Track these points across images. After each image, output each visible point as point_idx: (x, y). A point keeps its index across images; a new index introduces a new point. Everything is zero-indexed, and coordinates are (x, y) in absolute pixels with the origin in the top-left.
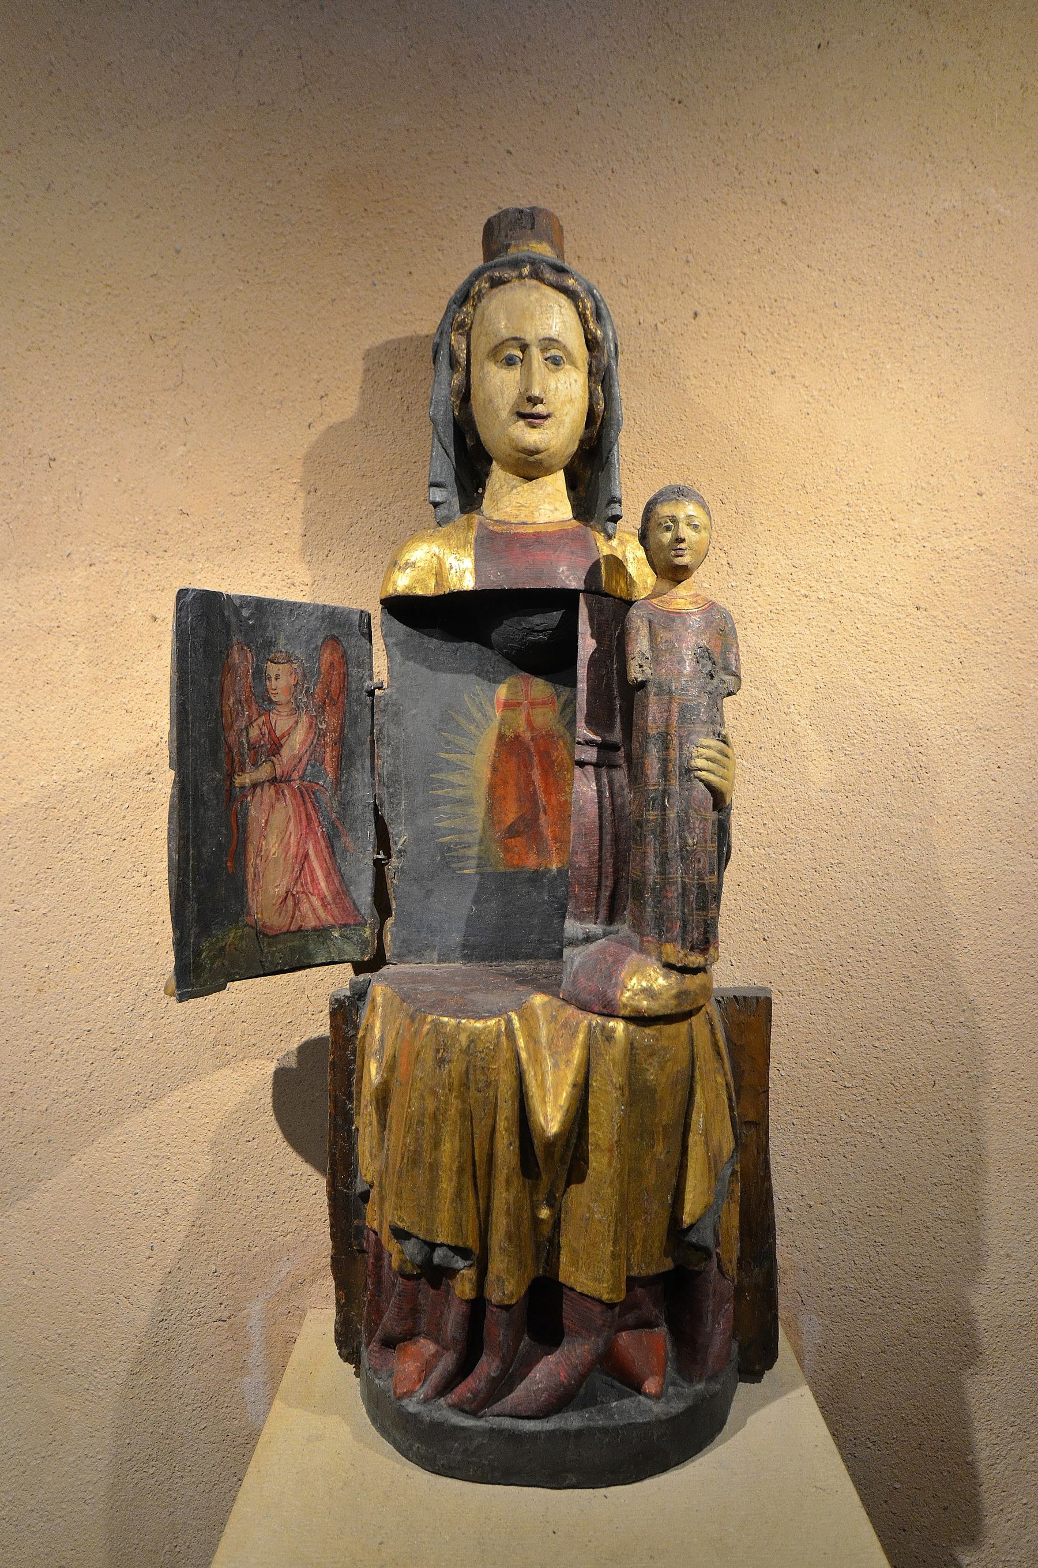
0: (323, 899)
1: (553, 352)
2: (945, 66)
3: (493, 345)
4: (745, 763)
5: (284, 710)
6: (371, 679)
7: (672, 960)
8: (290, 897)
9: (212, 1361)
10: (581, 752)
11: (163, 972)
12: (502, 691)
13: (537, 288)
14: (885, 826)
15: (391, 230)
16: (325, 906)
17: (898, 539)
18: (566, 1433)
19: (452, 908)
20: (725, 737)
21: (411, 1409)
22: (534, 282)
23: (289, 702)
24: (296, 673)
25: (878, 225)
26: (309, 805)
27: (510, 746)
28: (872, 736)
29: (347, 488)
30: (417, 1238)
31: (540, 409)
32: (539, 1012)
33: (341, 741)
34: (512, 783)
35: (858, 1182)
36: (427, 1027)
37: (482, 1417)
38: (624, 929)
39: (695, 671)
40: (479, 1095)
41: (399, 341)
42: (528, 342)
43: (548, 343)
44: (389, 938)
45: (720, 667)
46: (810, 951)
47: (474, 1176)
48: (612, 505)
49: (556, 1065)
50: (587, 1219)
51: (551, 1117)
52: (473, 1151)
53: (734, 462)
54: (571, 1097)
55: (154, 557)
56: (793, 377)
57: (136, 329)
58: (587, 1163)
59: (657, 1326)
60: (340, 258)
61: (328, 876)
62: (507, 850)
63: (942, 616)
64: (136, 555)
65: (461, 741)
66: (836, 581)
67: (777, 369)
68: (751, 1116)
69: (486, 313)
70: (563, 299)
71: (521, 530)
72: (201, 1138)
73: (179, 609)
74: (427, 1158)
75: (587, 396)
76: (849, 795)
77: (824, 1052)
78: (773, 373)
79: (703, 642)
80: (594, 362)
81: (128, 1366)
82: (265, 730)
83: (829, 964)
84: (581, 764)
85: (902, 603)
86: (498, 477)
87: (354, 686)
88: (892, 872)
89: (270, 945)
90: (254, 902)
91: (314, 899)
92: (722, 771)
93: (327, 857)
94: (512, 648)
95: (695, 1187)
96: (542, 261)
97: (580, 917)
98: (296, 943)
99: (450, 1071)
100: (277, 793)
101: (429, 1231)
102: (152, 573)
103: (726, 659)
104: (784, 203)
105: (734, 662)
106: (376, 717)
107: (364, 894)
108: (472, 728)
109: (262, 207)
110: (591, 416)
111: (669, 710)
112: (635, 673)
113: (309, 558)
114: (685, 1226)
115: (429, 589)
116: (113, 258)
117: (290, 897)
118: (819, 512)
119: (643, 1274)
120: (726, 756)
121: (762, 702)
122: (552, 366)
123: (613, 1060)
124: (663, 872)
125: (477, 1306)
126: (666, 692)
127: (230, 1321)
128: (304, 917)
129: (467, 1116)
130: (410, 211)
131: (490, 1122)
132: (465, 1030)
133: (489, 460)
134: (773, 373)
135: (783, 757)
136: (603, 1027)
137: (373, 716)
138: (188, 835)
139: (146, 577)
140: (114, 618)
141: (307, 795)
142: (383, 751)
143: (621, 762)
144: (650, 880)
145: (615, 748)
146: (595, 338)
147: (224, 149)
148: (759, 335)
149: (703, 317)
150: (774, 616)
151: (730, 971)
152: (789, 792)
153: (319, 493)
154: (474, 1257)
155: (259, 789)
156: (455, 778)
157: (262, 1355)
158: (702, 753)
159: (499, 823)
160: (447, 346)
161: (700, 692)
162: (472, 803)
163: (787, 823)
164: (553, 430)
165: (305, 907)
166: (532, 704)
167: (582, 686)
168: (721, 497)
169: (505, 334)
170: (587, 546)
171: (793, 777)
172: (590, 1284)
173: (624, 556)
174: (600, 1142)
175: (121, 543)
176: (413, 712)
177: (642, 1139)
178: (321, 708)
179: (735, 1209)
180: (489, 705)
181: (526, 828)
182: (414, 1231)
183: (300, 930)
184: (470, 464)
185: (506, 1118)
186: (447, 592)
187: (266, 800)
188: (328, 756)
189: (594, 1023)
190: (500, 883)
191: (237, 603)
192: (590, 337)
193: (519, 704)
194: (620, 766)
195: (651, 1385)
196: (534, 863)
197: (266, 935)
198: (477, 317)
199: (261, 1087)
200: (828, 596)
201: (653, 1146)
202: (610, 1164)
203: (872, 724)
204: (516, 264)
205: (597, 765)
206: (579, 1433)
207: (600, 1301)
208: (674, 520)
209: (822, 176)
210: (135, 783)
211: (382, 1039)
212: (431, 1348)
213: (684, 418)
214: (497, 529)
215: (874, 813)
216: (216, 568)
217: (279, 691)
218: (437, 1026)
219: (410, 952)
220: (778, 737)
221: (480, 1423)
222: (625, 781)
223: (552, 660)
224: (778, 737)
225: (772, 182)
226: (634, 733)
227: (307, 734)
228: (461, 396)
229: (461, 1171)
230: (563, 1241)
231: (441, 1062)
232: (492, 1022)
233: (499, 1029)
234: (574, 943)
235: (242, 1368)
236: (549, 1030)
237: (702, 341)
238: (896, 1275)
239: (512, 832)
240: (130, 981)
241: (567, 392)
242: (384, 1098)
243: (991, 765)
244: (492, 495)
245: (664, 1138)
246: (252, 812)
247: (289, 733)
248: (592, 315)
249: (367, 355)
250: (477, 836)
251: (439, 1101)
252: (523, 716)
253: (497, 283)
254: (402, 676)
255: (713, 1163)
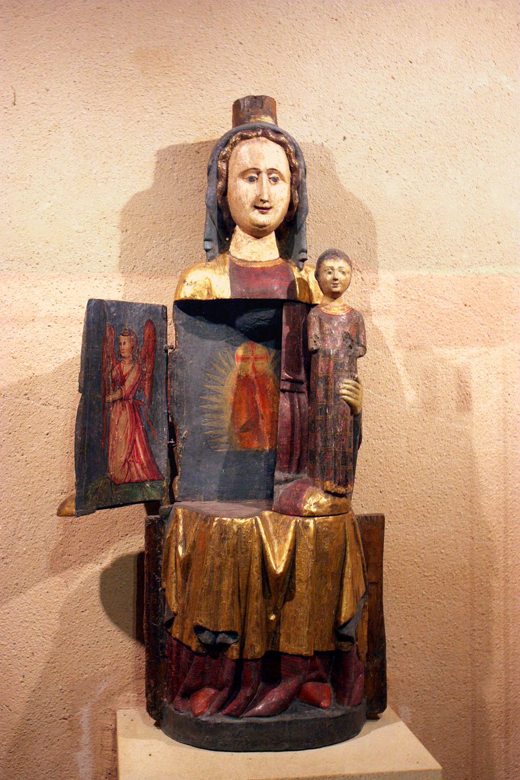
0: (142, 465)
1: (274, 175)
2: (479, 9)
3: (242, 170)
4: (370, 391)
5: (127, 361)
6: (167, 343)
7: (329, 489)
8: (127, 464)
9: (58, 743)
10: (284, 385)
11: (32, 512)
12: (240, 352)
13: (266, 142)
14: (447, 428)
15: (173, 83)
16: (142, 469)
17: (455, 266)
18: (284, 722)
19: (212, 472)
20: (357, 378)
21: (204, 719)
22: (264, 139)
23: (129, 357)
24: (133, 341)
25: (444, 93)
26: (137, 413)
27: (244, 381)
28: (440, 377)
29: (145, 230)
30: (209, 630)
31: (267, 205)
32: (268, 519)
33: (152, 379)
34: (244, 402)
35: (432, 630)
36: (215, 524)
37: (242, 718)
38: (305, 476)
39: (343, 345)
40: (242, 555)
41: (177, 146)
42: (261, 171)
43: (271, 171)
44: (177, 487)
45: (355, 339)
46: (406, 498)
47: (239, 597)
48: (302, 253)
49: (279, 542)
50: (295, 617)
51: (278, 566)
52: (239, 584)
53: (365, 221)
54: (288, 556)
55: (30, 267)
56: (398, 174)
57: (22, 134)
58: (295, 590)
59: (326, 682)
60: (142, 97)
61: (145, 453)
62: (241, 439)
63: (480, 311)
64: (19, 266)
65: (218, 378)
66: (421, 289)
67: (389, 170)
68: (374, 579)
69: (239, 153)
70: (278, 147)
71: (254, 266)
72: (54, 611)
73: (88, 310)
74: (215, 588)
75: (290, 195)
76: (428, 410)
77: (414, 556)
78: (387, 172)
79: (347, 330)
80: (294, 179)
81: (7, 747)
82: (119, 372)
83: (417, 506)
84: (284, 391)
85: (457, 302)
86: (239, 236)
87: (158, 347)
88: (451, 453)
89: (116, 489)
90: (111, 466)
91: (138, 465)
92: (355, 396)
93: (145, 442)
94: (247, 328)
95: (347, 604)
96: (268, 128)
97: (282, 470)
98: (127, 489)
99: (228, 544)
100: (123, 406)
101: (216, 626)
102: (29, 277)
103: (358, 338)
104: (393, 78)
105: (363, 340)
106: (169, 364)
107: (163, 463)
108: (223, 371)
109: (98, 67)
110: (291, 205)
111: (329, 365)
112: (312, 346)
113: (123, 270)
114: (342, 624)
115: (204, 296)
116: (9, 92)
117: (127, 464)
118: (412, 251)
119: (320, 650)
120: (358, 388)
121: (380, 357)
122: (272, 182)
123: (309, 538)
124: (325, 446)
125: (240, 663)
126: (326, 354)
127: (69, 719)
128: (132, 474)
129: (236, 565)
130: (184, 74)
131: (248, 569)
132: (235, 523)
133: (235, 225)
134: (387, 172)
135: (392, 388)
136: (303, 523)
137: (167, 364)
138: (85, 427)
139: (26, 279)
140: (6, 303)
141: (135, 408)
142: (175, 384)
143: (304, 390)
144: (319, 449)
145: (301, 383)
146: (295, 166)
147: (76, 32)
148: (379, 150)
149: (348, 140)
150: (387, 308)
151: (363, 501)
152: (395, 408)
153: (128, 232)
154: (238, 637)
155: (115, 405)
156: (213, 399)
157: (88, 739)
158: (345, 387)
159: (237, 424)
160: (216, 167)
161: (344, 356)
162: (223, 412)
163: (394, 425)
164: (273, 215)
165: (133, 469)
166: (256, 358)
167: (284, 350)
168: (358, 240)
169: (250, 166)
170: (286, 272)
171: (397, 399)
172: (296, 648)
173: (308, 279)
174: (302, 578)
175: (11, 259)
176: (191, 362)
177: (321, 579)
178: (144, 360)
179: (365, 626)
180: (239, 360)
181: (251, 427)
182: (208, 626)
183: (130, 482)
184: (224, 225)
185: (256, 566)
186: (215, 298)
187: (118, 409)
188: (146, 386)
189: (298, 521)
190: (238, 457)
191: (109, 304)
192: (292, 166)
193: (248, 358)
194: (304, 392)
195: (324, 703)
196: (256, 446)
197: (115, 484)
198: (233, 154)
199: (91, 579)
200: (417, 298)
201: (326, 583)
202: (307, 588)
203: (440, 370)
204: (254, 129)
205: (291, 391)
206: (290, 723)
207: (301, 656)
208: (332, 268)
209: (414, 65)
210: (17, 400)
211: (184, 535)
212: (212, 691)
213: (338, 195)
214: (241, 264)
215: (442, 420)
216: (68, 275)
217: (125, 351)
218: (220, 523)
219: (189, 494)
220: (389, 377)
221: (241, 721)
222: (306, 401)
223: (267, 335)
224: (389, 377)
225: (387, 67)
226: (311, 376)
227: (138, 373)
228: (222, 193)
229: (233, 592)
230: (282, 631)
231: (223, 540)
232: (249, 520)
233: (252, 523)
234: (280, 483)
235: (76, 746)
236: (274, 527)
237: (348, 153)
238: (453, 682)
239: (245, 429)
240: (12, 517)
241: (279, 195)
242: (188, 564)
243: (505, 393)
244: (236, 244)
245: (332, 579)
246: (112, 416)
247: (128, 374)
248: (293, 152)
249: (158, 153)
250: (226, 431)
251: (222, 559)
252: (251, 365)
253: (244, 138)
254: (185, 342)
255: (355, 593)
